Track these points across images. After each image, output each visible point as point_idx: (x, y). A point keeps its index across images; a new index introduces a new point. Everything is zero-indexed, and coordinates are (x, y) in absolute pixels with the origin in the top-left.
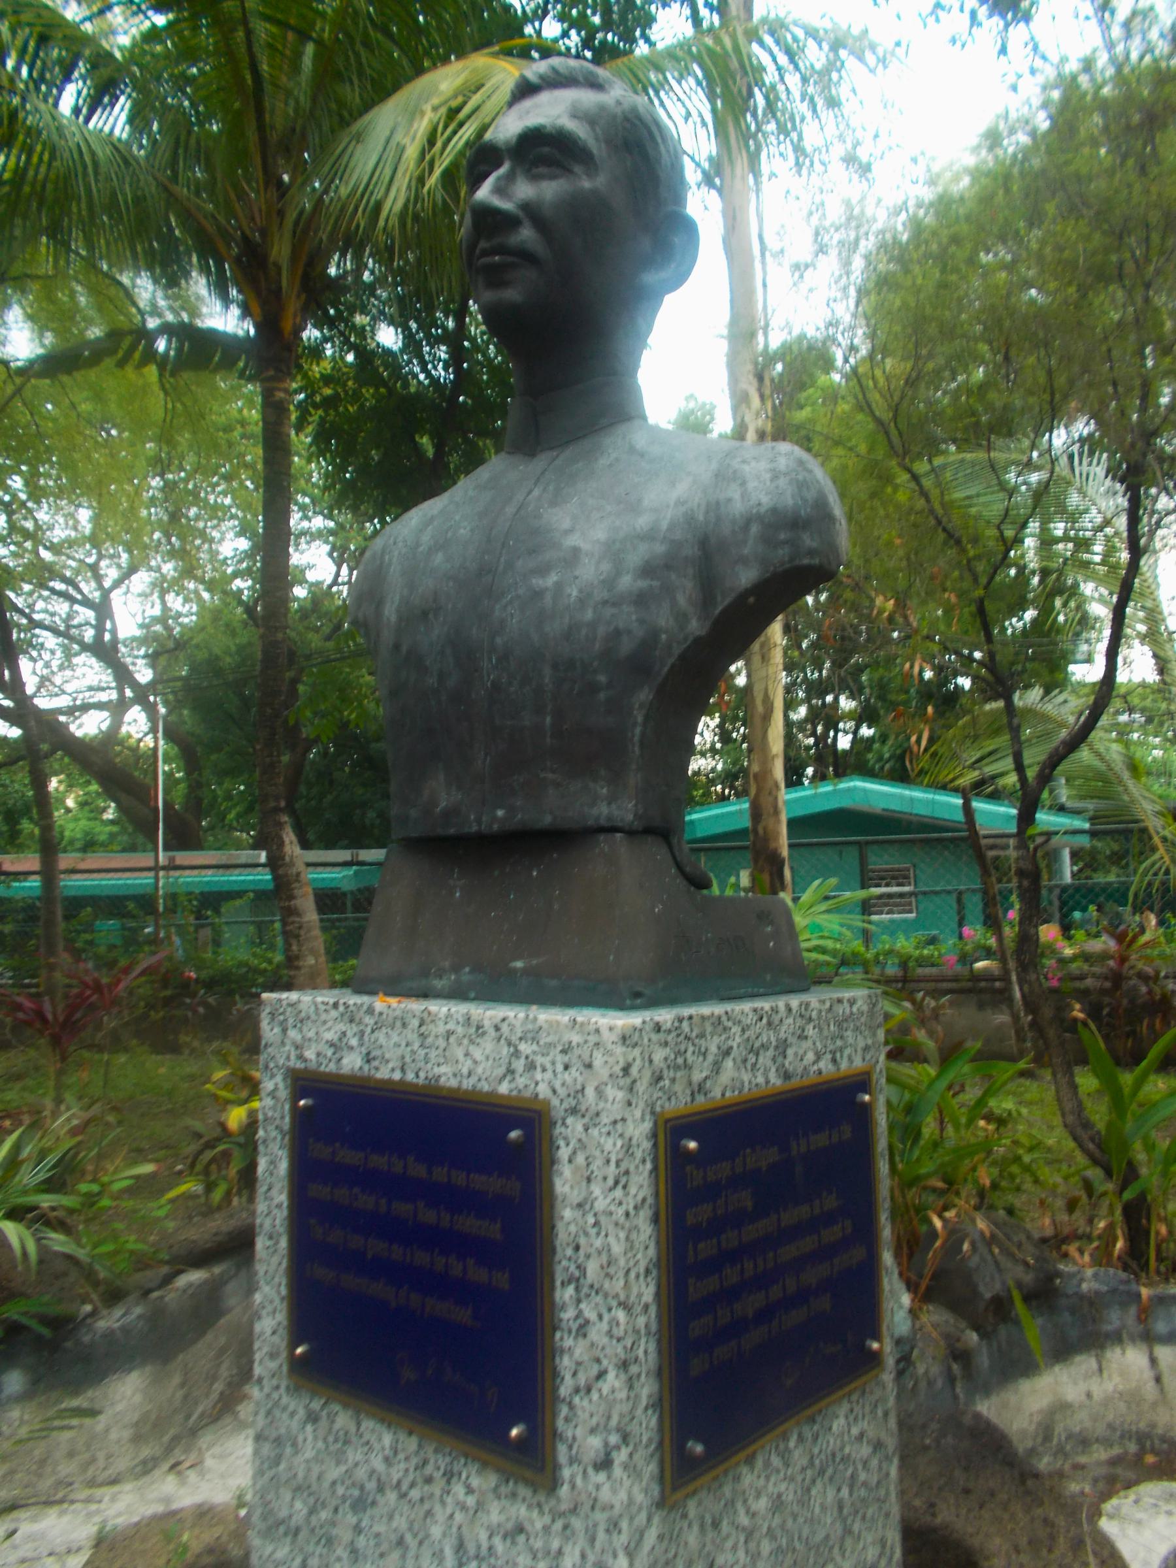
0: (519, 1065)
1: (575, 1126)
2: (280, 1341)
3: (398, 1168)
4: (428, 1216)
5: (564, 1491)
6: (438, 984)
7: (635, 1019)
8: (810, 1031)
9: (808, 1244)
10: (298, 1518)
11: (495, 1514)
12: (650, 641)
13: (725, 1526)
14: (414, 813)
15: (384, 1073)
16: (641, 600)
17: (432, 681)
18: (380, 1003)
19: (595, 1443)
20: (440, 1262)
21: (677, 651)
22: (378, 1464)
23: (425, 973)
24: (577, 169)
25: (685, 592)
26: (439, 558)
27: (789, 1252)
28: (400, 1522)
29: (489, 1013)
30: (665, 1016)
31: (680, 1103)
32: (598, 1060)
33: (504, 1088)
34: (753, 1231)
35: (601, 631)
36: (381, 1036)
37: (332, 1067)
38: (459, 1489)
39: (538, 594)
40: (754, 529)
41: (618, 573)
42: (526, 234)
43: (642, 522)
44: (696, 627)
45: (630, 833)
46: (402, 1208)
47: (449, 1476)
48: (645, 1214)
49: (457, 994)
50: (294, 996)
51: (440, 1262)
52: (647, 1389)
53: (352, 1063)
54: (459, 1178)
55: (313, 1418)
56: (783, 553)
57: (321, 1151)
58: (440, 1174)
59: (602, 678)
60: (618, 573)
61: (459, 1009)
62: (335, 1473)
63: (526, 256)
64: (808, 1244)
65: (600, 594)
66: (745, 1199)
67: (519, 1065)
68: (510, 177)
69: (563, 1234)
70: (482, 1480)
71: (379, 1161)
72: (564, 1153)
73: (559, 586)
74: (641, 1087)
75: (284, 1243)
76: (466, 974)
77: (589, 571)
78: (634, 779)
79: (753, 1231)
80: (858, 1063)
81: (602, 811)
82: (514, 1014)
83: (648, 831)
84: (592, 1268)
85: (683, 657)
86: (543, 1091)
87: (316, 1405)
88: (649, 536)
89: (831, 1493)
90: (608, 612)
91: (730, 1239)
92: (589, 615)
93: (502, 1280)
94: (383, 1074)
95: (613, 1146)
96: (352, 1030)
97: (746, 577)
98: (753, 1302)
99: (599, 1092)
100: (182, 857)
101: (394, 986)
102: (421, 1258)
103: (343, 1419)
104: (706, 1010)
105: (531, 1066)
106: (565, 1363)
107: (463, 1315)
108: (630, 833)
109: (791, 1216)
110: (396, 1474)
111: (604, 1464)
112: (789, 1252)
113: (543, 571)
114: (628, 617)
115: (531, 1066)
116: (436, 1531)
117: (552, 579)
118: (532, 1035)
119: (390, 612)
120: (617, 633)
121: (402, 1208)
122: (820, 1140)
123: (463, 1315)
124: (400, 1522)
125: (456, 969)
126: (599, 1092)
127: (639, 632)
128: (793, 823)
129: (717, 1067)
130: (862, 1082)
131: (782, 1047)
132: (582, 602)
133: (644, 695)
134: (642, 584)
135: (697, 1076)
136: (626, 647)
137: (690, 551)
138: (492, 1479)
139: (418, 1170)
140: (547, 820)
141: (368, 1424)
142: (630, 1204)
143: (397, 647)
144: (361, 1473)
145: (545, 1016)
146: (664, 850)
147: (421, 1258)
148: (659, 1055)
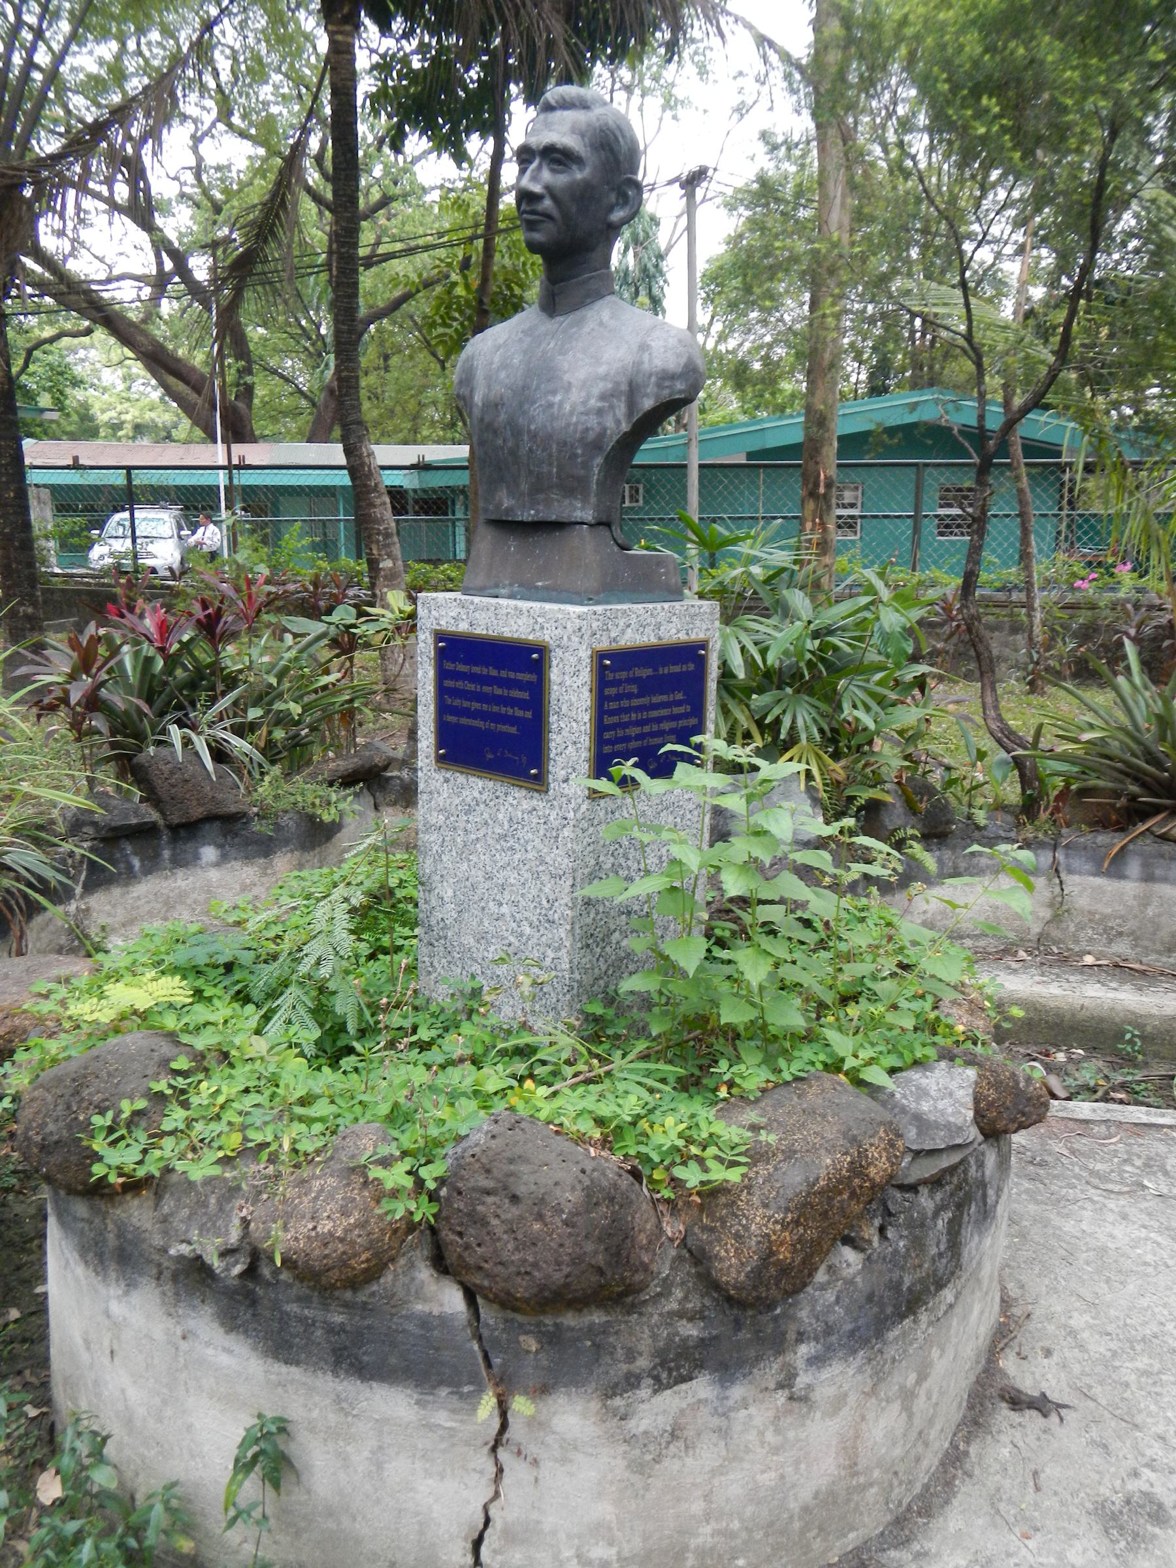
0: (537, 627)
1: (559, 652)
2: (432, 751)
3: (485, 672)
4: (498, 691)
5: (551, 792)
6: (503, 591)
7: (584, 609)
8: (674, 619)
9: (664, 712)
10: (441, 823)
11: (526, 805)
12: (602, 434)
13: (617, 814)
14: (491, 507)
15: (479, 631)
16: (600, 412)
17: (500, 442)
18: (477, 599)
19: (563, 772)
20: (503, 710)
21: (615, 438)
22: (476, 794)
23: (497, 586)
24: (574, 167)
25: (621, 409)
26: (503, 375)
27: (654, 714)
28: (486, 816)
29: (524, 605)
30: (599, 609)
31: (604, 645)
32: (569, 625)
33: (531, 637)
34: (636, 702)
35: (580, 428)
36: (477, 614)
37: (453, 629)
38: (510, 799)
39: (551, 405)
40: (653, 379)
41: (588, 398)
42: (547, 203)
43: (602, 370)
44: (625, 427)
45: (591, 525)
46: (487, 689)
47: (506, 794)
48: (587, 688)
49: (512, 596)
50: (434, 595)
51: (503, 710)
52: (585, 754)
53: (463, 627)
54: (512, 675)
55: (447, 781)
56: (666, 392)
57: (449, 666)
58: (504, 674)
59: (579, 451)
60: (588, 398)
61: (512, 602)
62: (457, 801)
63: (548, 216)
64: (664, 712)
65: (581, 409)
66: (634, 689)
67: (537, 627)
68: (539, 168)
69: (553, 696)
70: (519, 793)
71: (476, 670)
72: (554, 663)
73: (561, 403)
74: (586, 637)
75: (432, 707)
76: (516, 588)
77: (576, 396)
78: (593, 500)
79: (636, 702)
80: (702, 636)
81: (578, 515)
82: (536, 605)
83: (599, 524)
84: (564, 708)
85: (618, 442)
86: (547, 638)
87: (448, 775)
88: (604, 378)
89: (671, 818)
90: (584, 418)
91: (625, 703)
92: (574, 419)
93: (529, 715)
94: (478, 631)
95: (573, 660)
96: (463, 611)
97: (648, 404)
98: (634, 731)
99: (569, 639)
100: (238, 449)
101: (481, 591)
102: (495, 709)
103: (461, 779)
104: (619, 607)
105: (542, 628)
106: (552, 745)
107: (513, 730)
108: (591, 525)
109: (657, 699)
110: (484, 797)
111: (566, 781)
112: (654, 714)
113: (554, 392)
114: (593, 421)
115: (542, 628)
116: (500, 816)
117: (558, 398)
118: (542, 614)
119: (478, 399)
120: (587, 430)
121: (487, 689)
122: (676, 669)
123: (513, 730)
124: (486, 816)
125: (511, 585)
126: (569, 639)
127: (597, 429)
128: (841, 439)
129: (623, 632)
130: (703, 645)
131: (658, 626)
132: (571, 413)
133: (599, 460)
134: (600, 404)
135: (613, 635)
136: (591, 436)
137: (624, 387)
138: (524, 792)
139: (494, 673)
140: (554, 518)
141: (472, 779)
142: (579, 683)
143: (482, 420)
144: (469, 800)
145: (548, 606)
146: (608, 534)
147: (495, 709)
148: (595, 625)
